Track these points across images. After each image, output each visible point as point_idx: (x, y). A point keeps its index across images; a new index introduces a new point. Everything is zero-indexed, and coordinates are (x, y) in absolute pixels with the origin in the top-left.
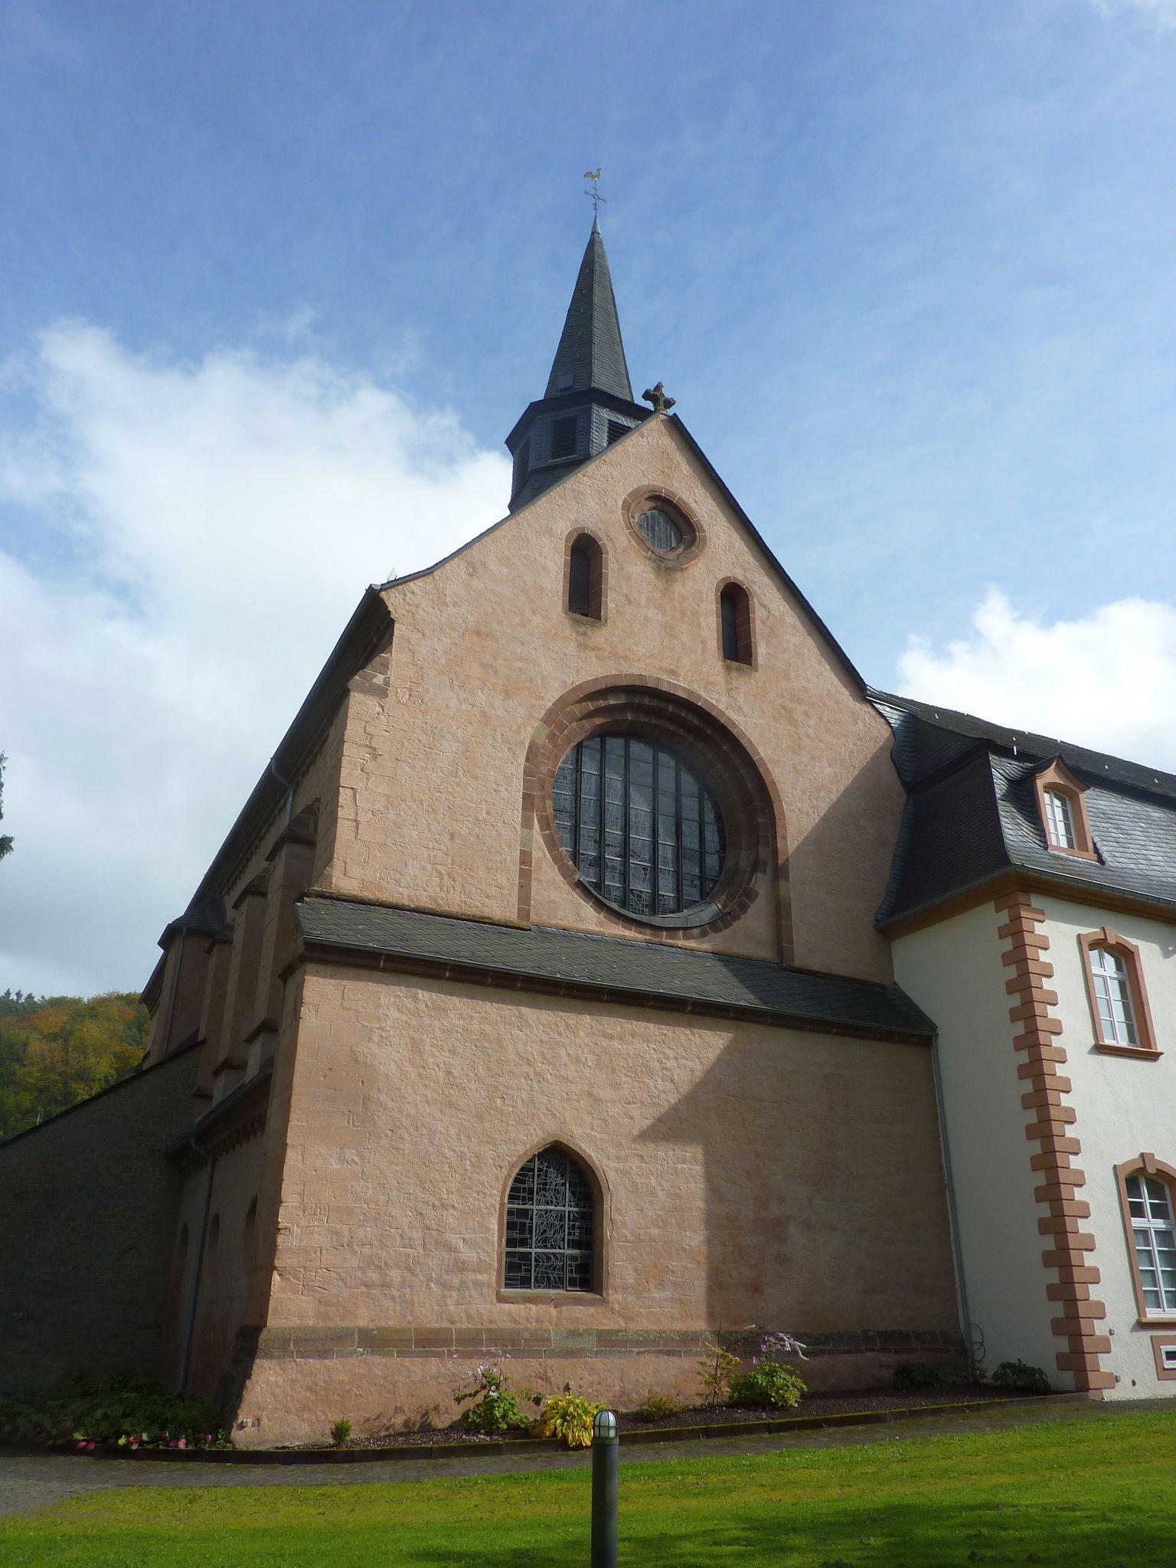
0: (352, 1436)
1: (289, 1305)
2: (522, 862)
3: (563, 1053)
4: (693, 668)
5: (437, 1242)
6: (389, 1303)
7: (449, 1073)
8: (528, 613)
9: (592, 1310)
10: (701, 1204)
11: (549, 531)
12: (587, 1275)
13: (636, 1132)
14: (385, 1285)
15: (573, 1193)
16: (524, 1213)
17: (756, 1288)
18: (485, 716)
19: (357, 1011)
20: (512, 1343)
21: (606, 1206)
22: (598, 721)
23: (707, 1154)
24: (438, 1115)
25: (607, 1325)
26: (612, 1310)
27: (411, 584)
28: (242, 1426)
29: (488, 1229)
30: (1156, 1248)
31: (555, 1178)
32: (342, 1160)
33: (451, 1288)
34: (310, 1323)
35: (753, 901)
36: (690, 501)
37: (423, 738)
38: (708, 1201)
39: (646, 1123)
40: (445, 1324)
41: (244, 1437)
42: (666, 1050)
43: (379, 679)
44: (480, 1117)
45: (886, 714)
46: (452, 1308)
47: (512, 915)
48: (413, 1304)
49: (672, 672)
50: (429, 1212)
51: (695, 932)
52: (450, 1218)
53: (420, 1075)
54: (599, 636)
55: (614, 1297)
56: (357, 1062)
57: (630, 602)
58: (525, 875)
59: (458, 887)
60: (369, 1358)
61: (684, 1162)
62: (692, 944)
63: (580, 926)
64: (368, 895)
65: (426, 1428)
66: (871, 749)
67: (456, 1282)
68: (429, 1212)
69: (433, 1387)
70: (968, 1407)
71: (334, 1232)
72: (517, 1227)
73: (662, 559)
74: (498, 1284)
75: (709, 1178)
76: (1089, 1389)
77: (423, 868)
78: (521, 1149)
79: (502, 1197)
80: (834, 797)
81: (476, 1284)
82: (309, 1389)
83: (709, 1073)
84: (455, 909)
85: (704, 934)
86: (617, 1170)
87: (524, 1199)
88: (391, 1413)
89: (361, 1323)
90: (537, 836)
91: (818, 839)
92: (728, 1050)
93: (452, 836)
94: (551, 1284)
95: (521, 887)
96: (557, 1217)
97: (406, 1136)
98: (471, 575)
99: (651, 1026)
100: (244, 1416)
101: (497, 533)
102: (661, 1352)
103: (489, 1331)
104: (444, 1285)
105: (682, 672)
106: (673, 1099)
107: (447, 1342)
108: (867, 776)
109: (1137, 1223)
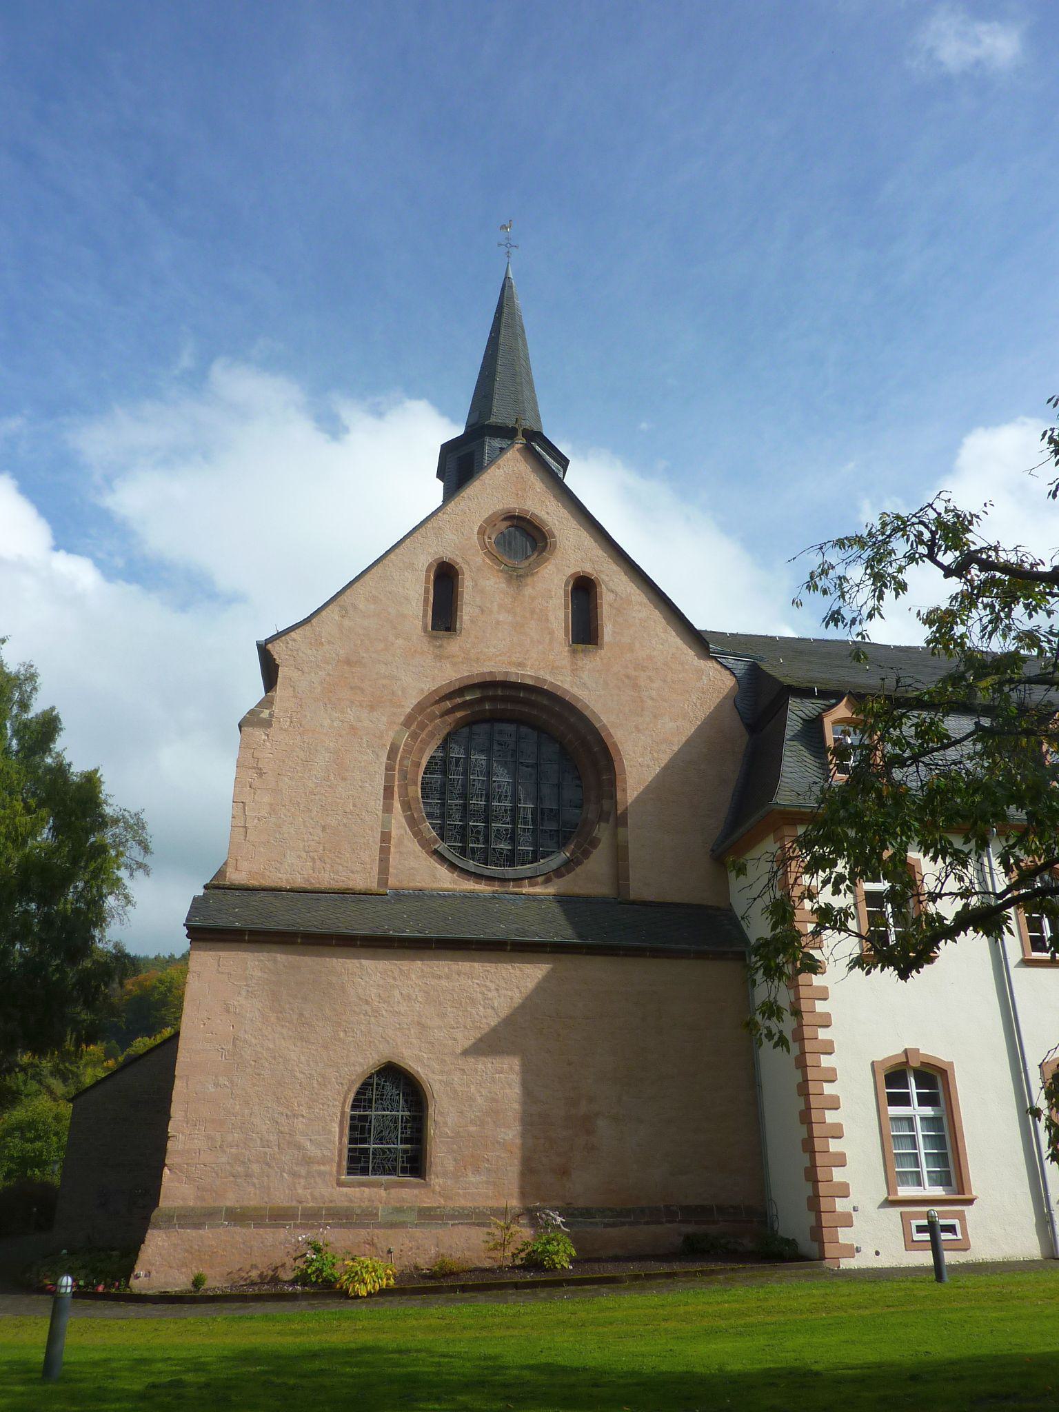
0: (206, 1286)
1: (176, 1189)
2: (383, 841)
3: (396, 993)
5: (289, 1143)
6: (252, 1189)
7: (301, 1015)
8: (391, 638)
9: (416, 1191)
10: (516, 1106)
11: (411, 567)
12: (416, 1165)
13: (459, 1051)
14: (248, 1175)
15: (406, 1101)
16: (364, 1119)
17: (564, 1172)
18: (353, 729)
19: (229, 974)
20: (345, 1218)
21: (431, 1111)
22: (459, 714)
23: (523, 1065)
24: (292, 1047)
25: (428, 1203)
26: (434, 1192)
27: (293, 634)
28: (137, 1277)
29: (330, 1132)
30: (920, 1132)
31: (390, 1090)
32: (216, 1085)
33: (300, 1176)
34: (191, 1204)
35: (595, 847)
36: (542, 514)
37: (301, 754)
38: (524, 1104)
39: (468, 1044)
40: (294, 1204)
41: (140, 1282)
42: (489, 984)
44: (325, 1047)
45: (729, 666)
46: (300, 1191)
47: (373, 885)
48: (269, 1188)
50: (283, 1120)
51: (540, 879)
52: (299, 1124)
53: (278, 1018)
54: (454, 646)
55: (435, 1181)
56: (228, 1012)
57: (483, 611)
58: (385, 851)
59: (328, 867)
60: (232, 1228)
61: (501, 1072)
62: (538, 890)
63: (436, 886)
64: (255, 883)
65: (275, 1280)
66: (713, 700)
67: (303, 1172)
68: (283, 1120)
69: (275, 1248)
70: (700, 1272)
71: (209, 1138)
72: (358, 1129)
73: (515, 569)
74: (339, 1173)
75: (524, 1085)
76: (824, 1258)
77: (299, 857)
78: (359, 1069)
79: (343, 1107)
80: (676, 749)
81: (320, 1174)
82: (187, 1251)
83: (528, 998)
84: (324, 885)
85: (548, 881)
86: (440, 1081)
87: (364, 1107)
88: (248, 1268)
89: (228, 1204)
91: (658, 789)
92: (546, 979)
93: (324, 828)
94: (385, 1172)
95: (381, 860)
96: (390, 1121)
97: (267, 1065)
98: (343, 617)
99: (476, 964)
100: (139, 1270)
101: (367, 577)
102: (473, 1224)
103: (328, 1209)
104: (294, 1175)
105: (529, 663)
106: (493, 1022)
107: (294, 1217)
108: (712, 721)
109: (895, 1111)
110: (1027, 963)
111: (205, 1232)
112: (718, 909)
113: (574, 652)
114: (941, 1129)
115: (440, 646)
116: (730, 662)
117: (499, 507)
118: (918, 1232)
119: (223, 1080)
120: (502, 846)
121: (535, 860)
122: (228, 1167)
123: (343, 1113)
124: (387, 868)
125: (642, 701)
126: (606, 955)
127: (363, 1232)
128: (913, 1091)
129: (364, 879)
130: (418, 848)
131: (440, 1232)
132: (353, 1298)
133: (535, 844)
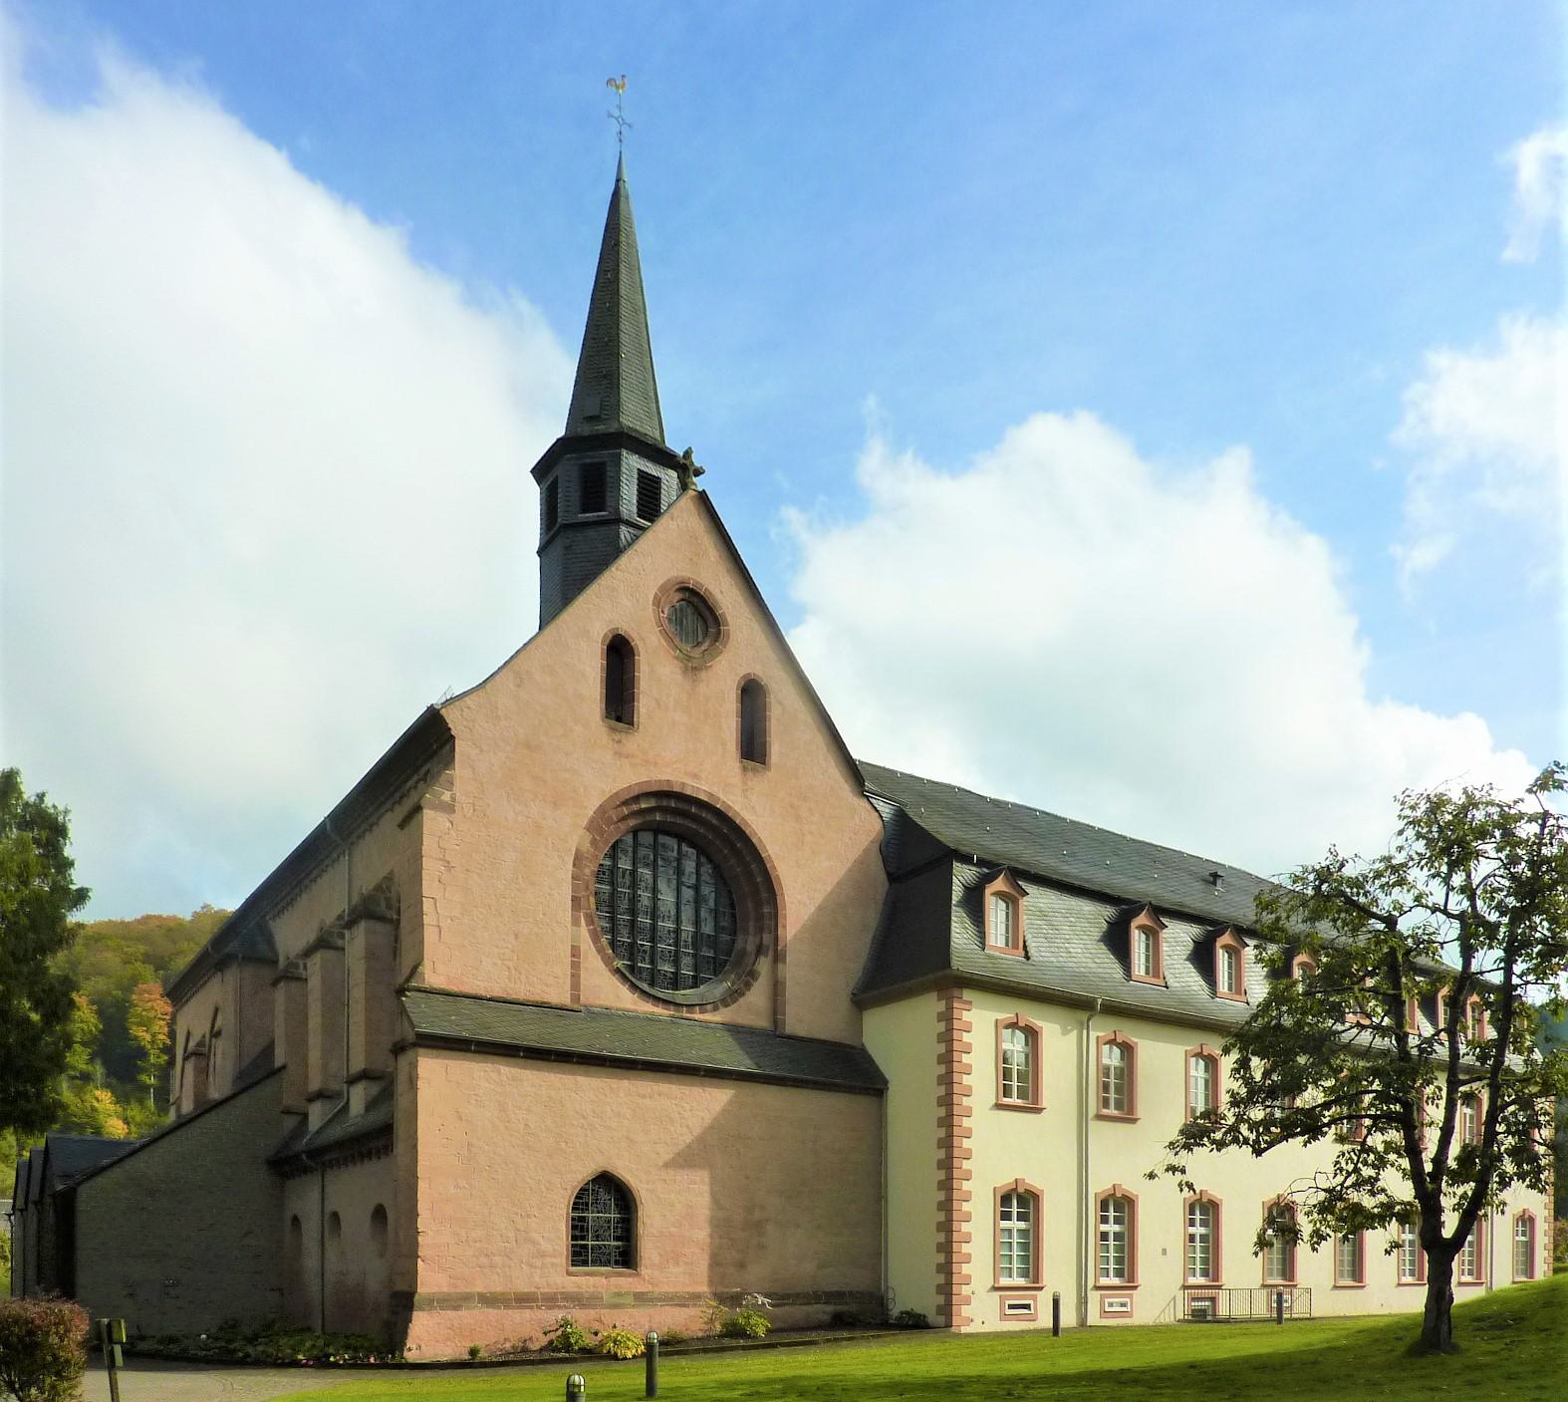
2: (573, 956)
4: (709, 771)
5: (525, 1239)
9: (630, 1280)
10: (707, 1212)
15: (616, 1205)
17: (742, 1265)
24: (521, 1155)
25: (640, 1289)
27: (466, 699)
28: (410, 1349)
30: (1016, 1239)
31: (603, 1196)
32: (457, 1186)
33: (535, 1267)
34: (445, 1290)
39: (668, 1157)
40: (533, 1290)
43: (446, 797)
48: (511, 1277)
49: (695, 776)
51: (709, 1007)
53: (507, 1127)
54: (633, 742)
55: (644, 1271)
56: (460, 1119)
59: (523, 977)
62: (707, 1017)
65: (525, 1350)
67: (539, 1264)
69: (530, 1326)
72: (578, 1228)
75: (713, 1194)
78: (580, 1177)
84: (521, 996)
85: (716, 1009)
86: (647, 1190)
87: (582, 1209)
88: (502, 1341)
90: (584, 932)
92: (731, 1102)
95: (573, 975)
96: (606, 1221)
98: (518, 686)
99: (673, 1086)
102: (676, 1305)
103: (562, 1293)
106: (688, 1139)
107: (536, 1300)
108: (861, 862)
109: (1005, 1224)
110: (1100, 1117)
111: (463, 1313)
112: (853, 1047)
113: (745, 769)
114: (1027, 1237)
115: (619, 742)
116: (881, 805)
117: (674, 573)
118: (1030, 1305)
119: (462, 1183)
120: (666, 968)
121: (695, 985)
122: (474, 1259)
123: (568, 1214)
124: (578, 983)
125: (803, 834)
126: (830, 1090)
127: (592, 1312)
128: (1015, 1210)
129: (558, 993)
130: (601, 965)
131: (651, 1311)
132: (622, 1360)
133: (696, 968)
